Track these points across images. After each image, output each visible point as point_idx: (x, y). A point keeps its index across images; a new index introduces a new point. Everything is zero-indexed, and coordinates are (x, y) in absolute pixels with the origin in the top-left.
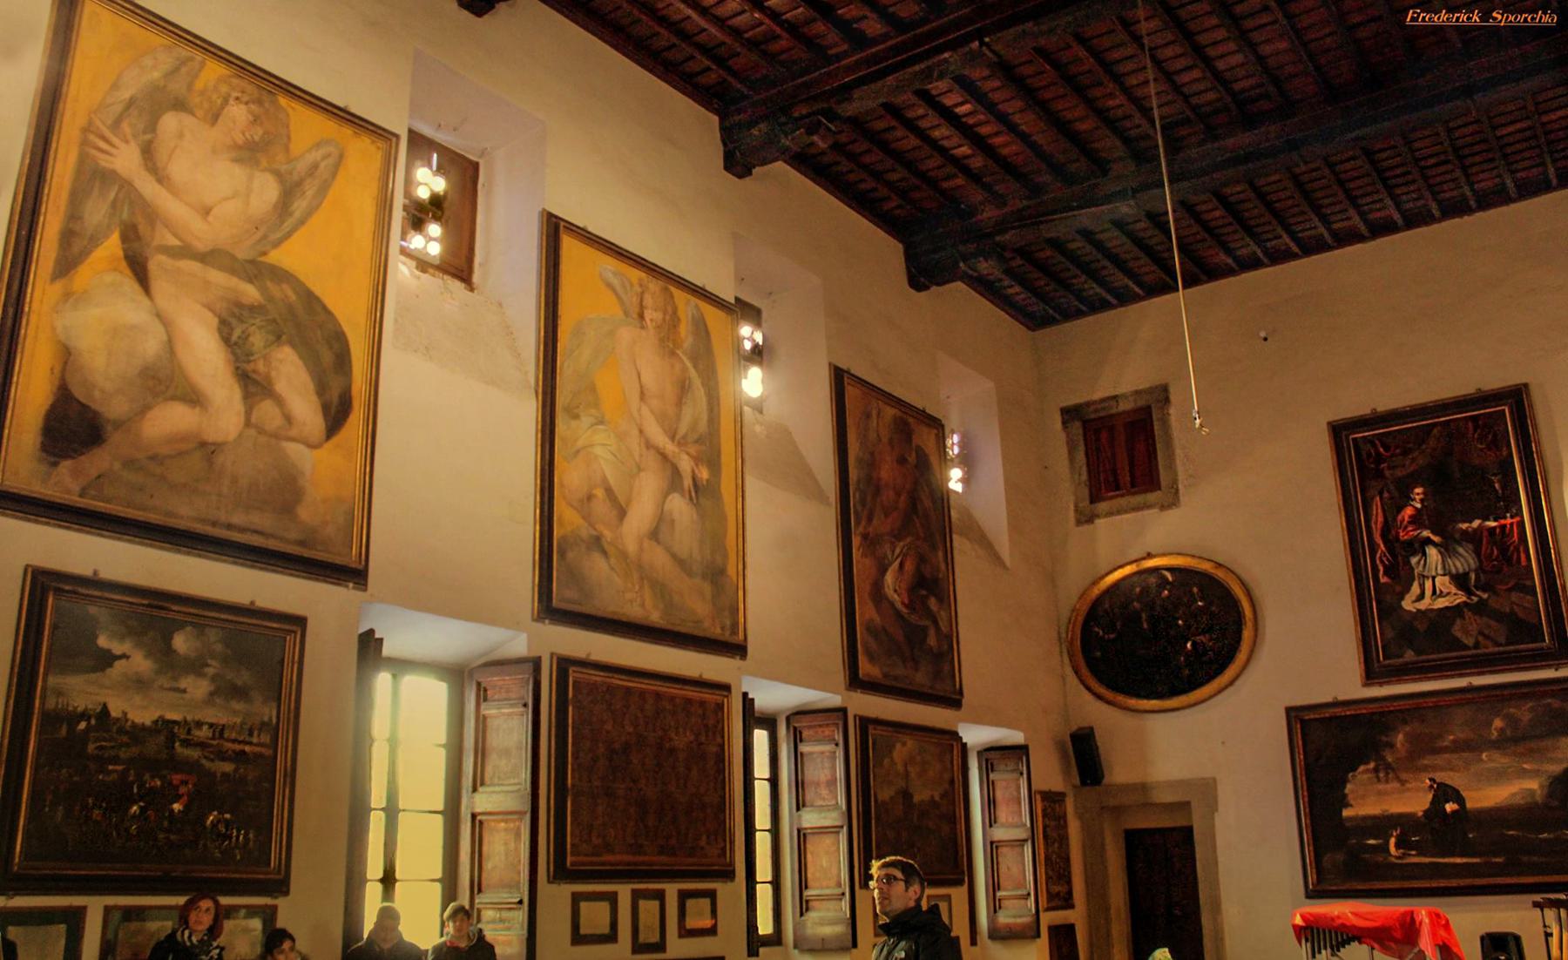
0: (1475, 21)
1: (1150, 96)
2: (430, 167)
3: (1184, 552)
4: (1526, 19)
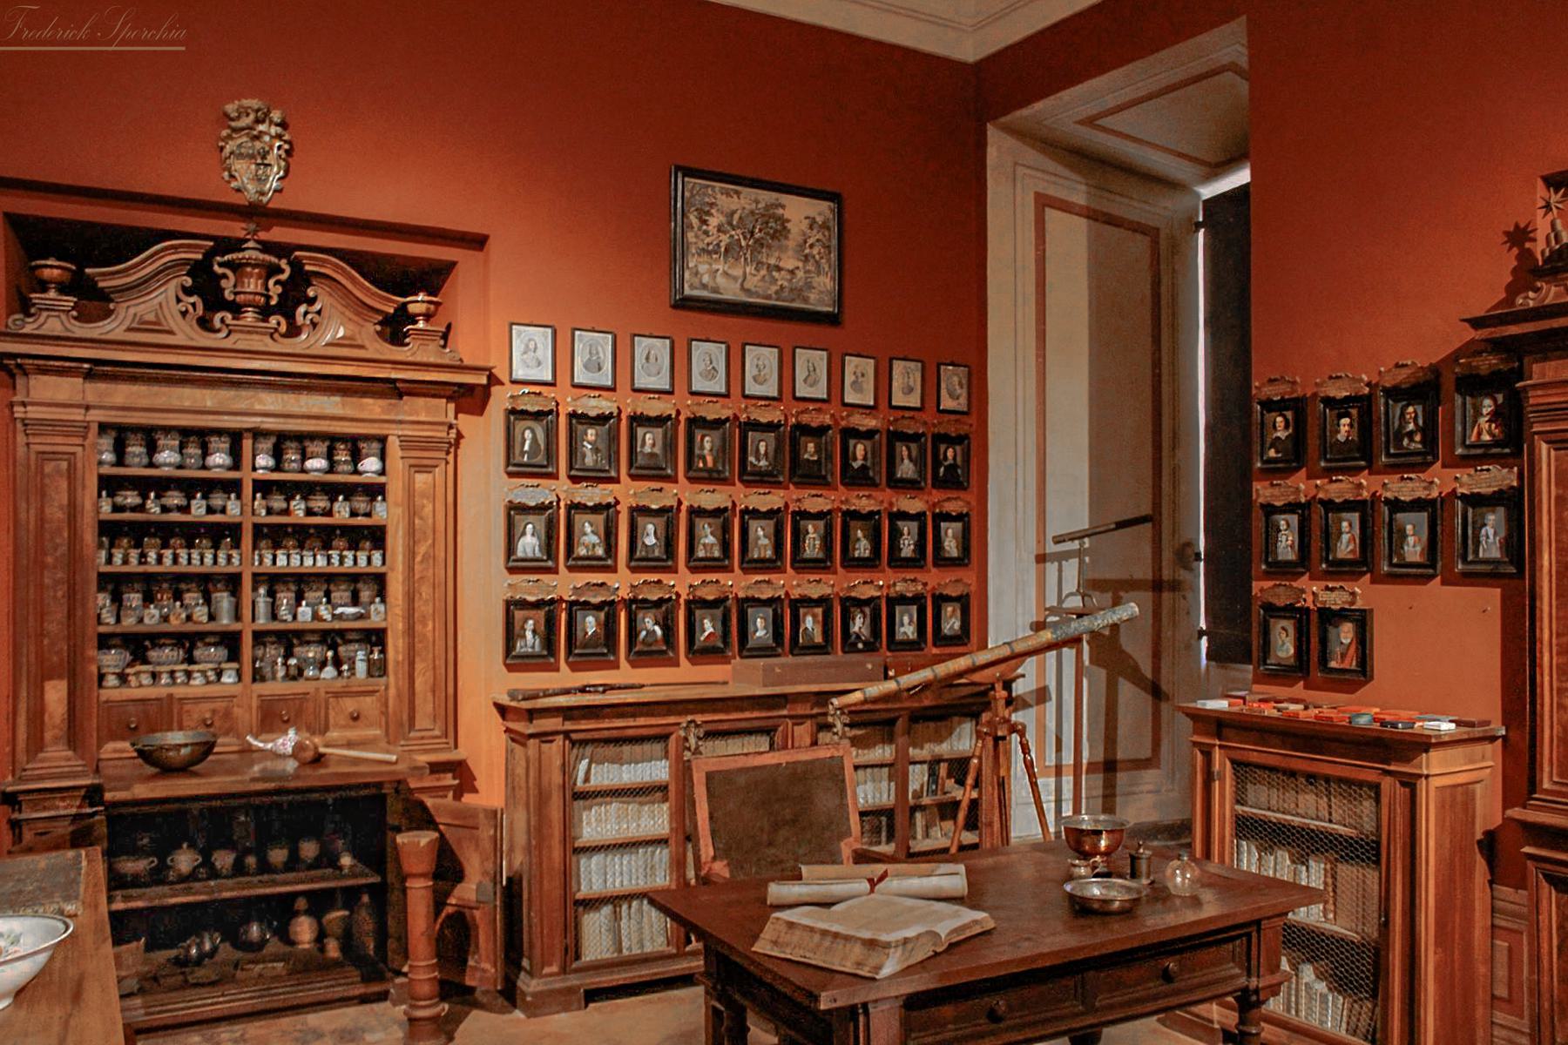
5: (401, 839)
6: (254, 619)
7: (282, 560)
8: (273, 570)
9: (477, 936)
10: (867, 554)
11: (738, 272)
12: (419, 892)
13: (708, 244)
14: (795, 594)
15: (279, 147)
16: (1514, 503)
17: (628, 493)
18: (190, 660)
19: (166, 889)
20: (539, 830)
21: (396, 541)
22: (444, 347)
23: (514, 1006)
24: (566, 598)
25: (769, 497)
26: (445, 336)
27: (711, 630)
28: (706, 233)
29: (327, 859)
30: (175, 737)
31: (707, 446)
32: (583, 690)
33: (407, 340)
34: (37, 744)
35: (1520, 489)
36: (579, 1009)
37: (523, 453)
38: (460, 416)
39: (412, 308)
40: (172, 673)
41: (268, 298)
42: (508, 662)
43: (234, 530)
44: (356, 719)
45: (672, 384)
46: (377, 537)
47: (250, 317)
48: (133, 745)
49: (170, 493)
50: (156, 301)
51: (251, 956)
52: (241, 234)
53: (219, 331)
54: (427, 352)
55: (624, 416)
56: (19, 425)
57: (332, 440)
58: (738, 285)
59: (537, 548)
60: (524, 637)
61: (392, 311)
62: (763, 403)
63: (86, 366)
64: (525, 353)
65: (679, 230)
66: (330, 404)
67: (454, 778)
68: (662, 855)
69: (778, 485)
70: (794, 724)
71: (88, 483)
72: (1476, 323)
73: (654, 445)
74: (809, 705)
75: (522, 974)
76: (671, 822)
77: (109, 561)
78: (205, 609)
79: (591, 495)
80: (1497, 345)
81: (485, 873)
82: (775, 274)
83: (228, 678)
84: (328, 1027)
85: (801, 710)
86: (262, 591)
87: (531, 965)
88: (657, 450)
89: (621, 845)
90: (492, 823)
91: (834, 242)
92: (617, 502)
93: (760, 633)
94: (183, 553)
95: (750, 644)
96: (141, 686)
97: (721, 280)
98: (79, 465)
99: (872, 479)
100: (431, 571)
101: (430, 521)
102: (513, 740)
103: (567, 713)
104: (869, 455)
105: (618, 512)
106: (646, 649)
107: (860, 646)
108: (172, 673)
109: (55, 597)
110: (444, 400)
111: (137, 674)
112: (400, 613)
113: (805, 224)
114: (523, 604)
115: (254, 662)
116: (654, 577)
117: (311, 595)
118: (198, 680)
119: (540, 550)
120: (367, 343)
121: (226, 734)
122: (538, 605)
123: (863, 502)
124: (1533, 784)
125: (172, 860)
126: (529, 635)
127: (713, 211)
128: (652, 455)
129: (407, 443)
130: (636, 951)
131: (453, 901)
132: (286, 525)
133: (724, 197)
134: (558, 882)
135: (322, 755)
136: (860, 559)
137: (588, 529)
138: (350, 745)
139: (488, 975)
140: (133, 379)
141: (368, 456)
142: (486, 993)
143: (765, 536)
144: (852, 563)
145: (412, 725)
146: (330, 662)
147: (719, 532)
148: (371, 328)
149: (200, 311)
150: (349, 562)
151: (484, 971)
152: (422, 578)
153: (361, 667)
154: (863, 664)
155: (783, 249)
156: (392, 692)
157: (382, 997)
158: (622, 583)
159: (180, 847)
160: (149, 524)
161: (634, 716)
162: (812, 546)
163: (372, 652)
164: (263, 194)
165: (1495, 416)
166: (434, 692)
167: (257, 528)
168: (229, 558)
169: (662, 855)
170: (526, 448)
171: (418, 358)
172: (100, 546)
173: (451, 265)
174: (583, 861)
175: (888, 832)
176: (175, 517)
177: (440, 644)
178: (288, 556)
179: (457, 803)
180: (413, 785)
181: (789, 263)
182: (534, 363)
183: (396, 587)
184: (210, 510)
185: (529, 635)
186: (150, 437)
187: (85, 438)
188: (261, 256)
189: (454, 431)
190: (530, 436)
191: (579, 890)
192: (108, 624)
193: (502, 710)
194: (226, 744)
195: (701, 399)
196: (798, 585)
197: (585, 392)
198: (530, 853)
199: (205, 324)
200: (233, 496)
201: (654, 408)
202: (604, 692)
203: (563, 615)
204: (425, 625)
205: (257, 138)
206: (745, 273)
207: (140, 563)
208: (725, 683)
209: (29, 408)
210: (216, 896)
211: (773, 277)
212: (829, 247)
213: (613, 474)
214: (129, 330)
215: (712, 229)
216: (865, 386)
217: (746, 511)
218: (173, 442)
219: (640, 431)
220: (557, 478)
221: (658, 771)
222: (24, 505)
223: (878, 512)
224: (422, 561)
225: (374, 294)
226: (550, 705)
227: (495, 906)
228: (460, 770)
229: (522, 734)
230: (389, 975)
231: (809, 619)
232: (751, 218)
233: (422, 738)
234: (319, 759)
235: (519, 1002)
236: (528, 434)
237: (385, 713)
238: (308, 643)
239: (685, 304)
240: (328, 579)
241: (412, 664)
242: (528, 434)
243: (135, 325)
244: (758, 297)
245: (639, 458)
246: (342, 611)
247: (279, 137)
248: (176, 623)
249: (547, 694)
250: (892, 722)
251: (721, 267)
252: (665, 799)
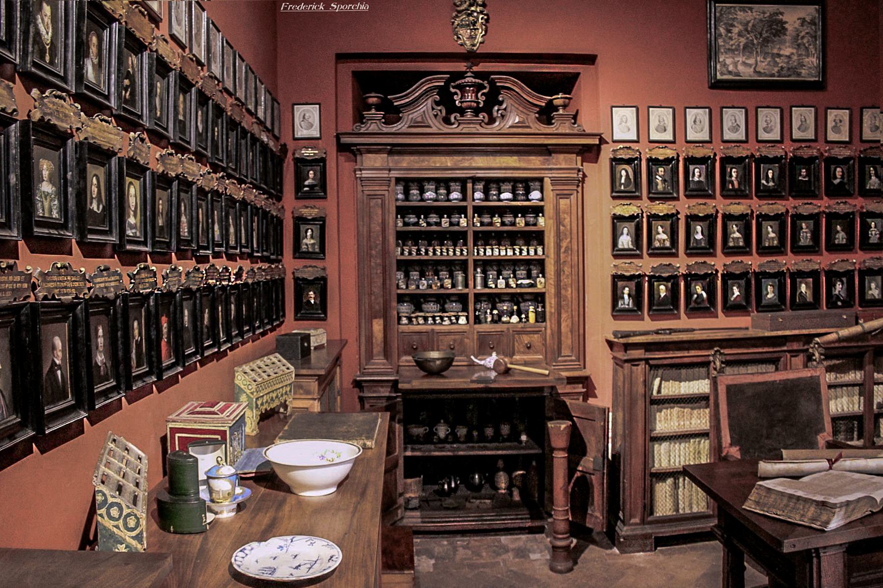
2: (153, 173)
4: (351, 7)
5: (550, 425)
6: (475, 287)
7: (489, 252)
8: (485, 258)
9: (593, 492)
10: (844, 241)
11: (751, 61)
12: (560, 458)
13: (732, 45)
14: (793, 269)
15: (482, 19)
17: (684, 206)
18: (443, 310)
19: (432, 447)
20: (629, 423)
21: (550, 239)
22: (574, 124)
23: (614, 545)
24: (648, 274)
25: (774, 206)
26: (575, 117)
27: (738, 293)
28: (731, 38)
29: (514, 436)
30: (434, 355)
31: (734, 175)
32: (657, 332)
33: (553, 121)
34: (370, 356)
36: (651, 550)
37: (621, 184)
38: (584, 164)
39: (556, 102)
40: (434, 318)
41: (478, 103)
42: (614, 314)
43: (463, 235)
44: (529, 348)
45: (711, 137)
46: (537, 237)
47: (469, 115)
48: (413, 357)
49: (431, 215)
50: (422, 110)
51: (475, 494)
52: (464, 69)
53: (453, 124)
54: (565, 128)
55: (681, 159)
56: (359, 180)
57: (515, 181)
58: (752, 70)
59: (630, 243)
60: (623, 298)
61: (544, 104)
62: (770, 145)
63: (389, 147)
64: (620, 124)
65: (713, 39)
66: (512, 161)
67: (583, 388)
68: (705, 445)
69: (781, 198)
70: (792, 356)
71: (391, 211)
73: (700, 176)
74: (801, 343)
75: (619, 523)
76: (710, 422)
77: (402, 254)
78: (450, 281)
79: (661, 208)
81: (598, 451)
82: (777, 60)
83: (462, 320)
84: (511, 546)
85: (795, 346)
86: (479, 270)
87: (624, 516)
88: (702, 179)
89: (679, 436)
90: (603, 417)
91: (819, 33)
92: (678, 213)
93: (769, 296)
94: (438, 248)
95: (764, 302)
96: (419, 324)
97: (741, 68)
98: (387, 202)
99: (848, 191)
100: (570, 257)
101: (569, 227)
102: (617, 364)
103: (648, 347)
104: (846, 176)
105: (678, 219)
106: (696, 306)
107: (839, 303)
108: (434, 318)
109: (377, 273)
110: (575, 155)
111: (417, 317)
112: (553, 283)
113: (797, 24)
114: (622, 277)
115: (475, 313)
116: (701, 260)
117: (505, 273)
118: (447, 322)
119: (632, 244)
120: (531, 125)
121: (461, 355)
122: (631, 278)
123: (841, 207)
125: (436, 430)
126: (626, 296)
127: (735, 23)
128: (699, 182)
129: (555, 181)
130: (688, 511)
131: (580, 468)
132: (490, 232)
133: (742, 13)
134: (641, 460)
135: (510, 369)
136: (839, 245)
137: (660, 229)
138: (526, 364)
139: (599, 520)
140: (412, 153)
141: (534, 190)
142: (598, 533)
143: (773, 232)
144: (833, 248)
145: (559, 354)
146: (515, 313)
147: (742, 230)
148: (533, 116)
149: (444, 113)
150: (525, 253)
151: (596, 517)
152: (564, 262)
153: (532, 316)
154: (841, 315)
155: (783, 42)
156: (549, 331)
157: (540, 530)
158: (682, 264)
159: (440, 422)
160: (421, 232)
161: (688, 349)
162: (805, 237)
163: (538, 307)
164: (474, 45)
166: (571, 332)
167: (476, 234)
168: (462, 251)
169: (705, 445)
170: (623, 181)
171: (560, 131)
172: (398, 245)
173: (577, 75)
174: (656, 446)
175: (858, 431)
176: (434, 228)
177: (575, 303)
178: (492, 249)
179: (584, 404)
180: (560, 391)
181: (787, 51)
182: (626, 129)
183: (550, 268)
184: (451, 224)
185: (626, 296)
186: (421, 183)
187: (389, 186)
188: (474, 80)
189: (581, 173)
190: (624, 172)
191: (654, 466)
192: (402, 289)
193: (611, 344)
194: (459, 361)
195: (730, 145)
196: (796, 263)
197: (657, 145)
198: (625, 439)
199: (447, 121)
200: (463, 216)
201: (699, 153)
202: (670, 333)
203: (646, 284)
204: (566, 290)
205: (469, 15)
206: (756, 61)
207: (417, 254)
208: (747, 329)
209: (363, 172)
210: (456, 453)
211: (776, 62)
212: (815, 37)
213: (675, 195)
214: (410, 127)
215: (734, 36)
216: (842, 128)
217: (760, 216)
218: (431, 187)
219: (691, 167)
220: (642, 199)
221: (702, 386)
222: (361, 223)
223: (853, 213)
224: (564, 252)
225: (534, 96)
226: (637, 341)
227: (604, 473)
228: (585, 381)
229: (621, 360)
230: (545, 516)
231: (803, 286)
232: (760, 25)
233: (565, 361)
234: (507, 371)
235: (616, 542)
236: (624, 173)
237: (545, 345)
238: (504, 301)
239: (718, 85)
240: (514, 263)
241: (559, 314)
242: (624, 173)
243: (412, 124)
244: (766, 76)
245: (691, 185)
246: (518, 283)
247: (481, 12)
248: (435, 290)
249: (635, 334)
250: (861, 355)
251: (740, 59)
252: (707, 406)
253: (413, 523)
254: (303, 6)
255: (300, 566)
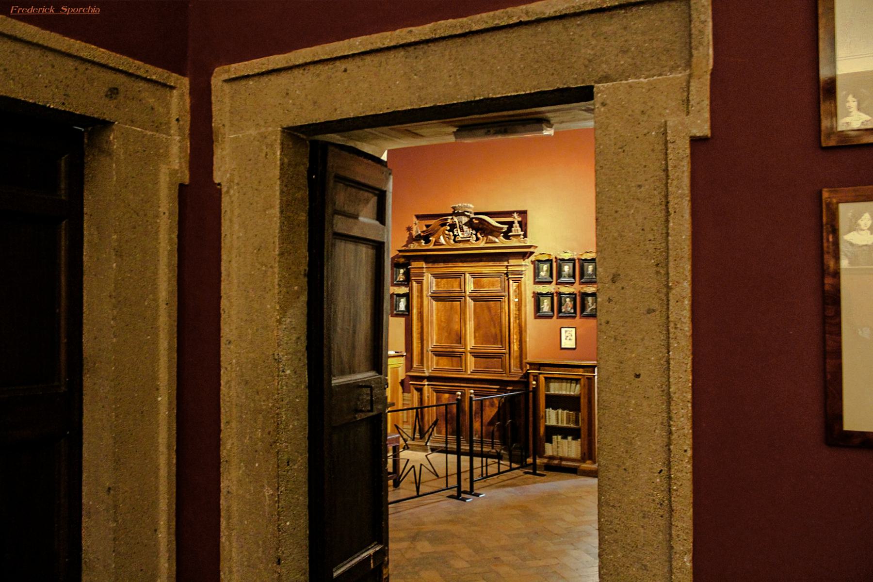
0: (52, 12)
1: (168, 123)
3: (459, 41)
4: (81, 10)
16: (407, 296)
35: (409, 293)
72: (400, 251)
80: (404, 257)
124: (412, 366)
165: (404, 274)
253: (345, 565)
254: (32, 9)
255: (595, 138)
